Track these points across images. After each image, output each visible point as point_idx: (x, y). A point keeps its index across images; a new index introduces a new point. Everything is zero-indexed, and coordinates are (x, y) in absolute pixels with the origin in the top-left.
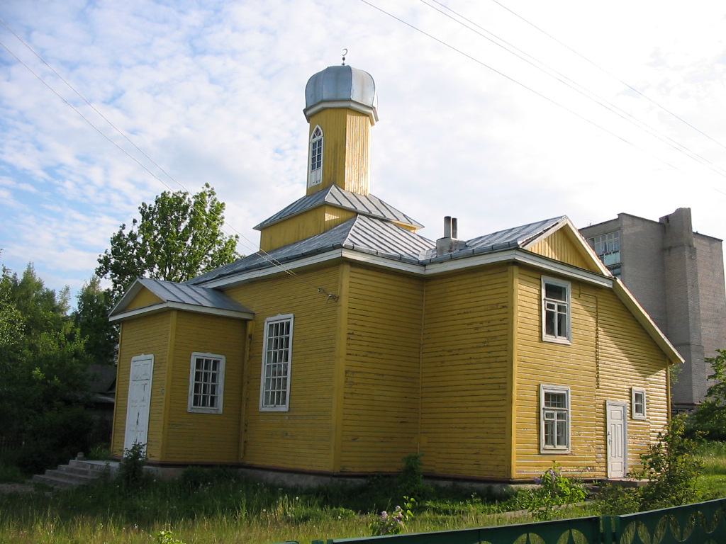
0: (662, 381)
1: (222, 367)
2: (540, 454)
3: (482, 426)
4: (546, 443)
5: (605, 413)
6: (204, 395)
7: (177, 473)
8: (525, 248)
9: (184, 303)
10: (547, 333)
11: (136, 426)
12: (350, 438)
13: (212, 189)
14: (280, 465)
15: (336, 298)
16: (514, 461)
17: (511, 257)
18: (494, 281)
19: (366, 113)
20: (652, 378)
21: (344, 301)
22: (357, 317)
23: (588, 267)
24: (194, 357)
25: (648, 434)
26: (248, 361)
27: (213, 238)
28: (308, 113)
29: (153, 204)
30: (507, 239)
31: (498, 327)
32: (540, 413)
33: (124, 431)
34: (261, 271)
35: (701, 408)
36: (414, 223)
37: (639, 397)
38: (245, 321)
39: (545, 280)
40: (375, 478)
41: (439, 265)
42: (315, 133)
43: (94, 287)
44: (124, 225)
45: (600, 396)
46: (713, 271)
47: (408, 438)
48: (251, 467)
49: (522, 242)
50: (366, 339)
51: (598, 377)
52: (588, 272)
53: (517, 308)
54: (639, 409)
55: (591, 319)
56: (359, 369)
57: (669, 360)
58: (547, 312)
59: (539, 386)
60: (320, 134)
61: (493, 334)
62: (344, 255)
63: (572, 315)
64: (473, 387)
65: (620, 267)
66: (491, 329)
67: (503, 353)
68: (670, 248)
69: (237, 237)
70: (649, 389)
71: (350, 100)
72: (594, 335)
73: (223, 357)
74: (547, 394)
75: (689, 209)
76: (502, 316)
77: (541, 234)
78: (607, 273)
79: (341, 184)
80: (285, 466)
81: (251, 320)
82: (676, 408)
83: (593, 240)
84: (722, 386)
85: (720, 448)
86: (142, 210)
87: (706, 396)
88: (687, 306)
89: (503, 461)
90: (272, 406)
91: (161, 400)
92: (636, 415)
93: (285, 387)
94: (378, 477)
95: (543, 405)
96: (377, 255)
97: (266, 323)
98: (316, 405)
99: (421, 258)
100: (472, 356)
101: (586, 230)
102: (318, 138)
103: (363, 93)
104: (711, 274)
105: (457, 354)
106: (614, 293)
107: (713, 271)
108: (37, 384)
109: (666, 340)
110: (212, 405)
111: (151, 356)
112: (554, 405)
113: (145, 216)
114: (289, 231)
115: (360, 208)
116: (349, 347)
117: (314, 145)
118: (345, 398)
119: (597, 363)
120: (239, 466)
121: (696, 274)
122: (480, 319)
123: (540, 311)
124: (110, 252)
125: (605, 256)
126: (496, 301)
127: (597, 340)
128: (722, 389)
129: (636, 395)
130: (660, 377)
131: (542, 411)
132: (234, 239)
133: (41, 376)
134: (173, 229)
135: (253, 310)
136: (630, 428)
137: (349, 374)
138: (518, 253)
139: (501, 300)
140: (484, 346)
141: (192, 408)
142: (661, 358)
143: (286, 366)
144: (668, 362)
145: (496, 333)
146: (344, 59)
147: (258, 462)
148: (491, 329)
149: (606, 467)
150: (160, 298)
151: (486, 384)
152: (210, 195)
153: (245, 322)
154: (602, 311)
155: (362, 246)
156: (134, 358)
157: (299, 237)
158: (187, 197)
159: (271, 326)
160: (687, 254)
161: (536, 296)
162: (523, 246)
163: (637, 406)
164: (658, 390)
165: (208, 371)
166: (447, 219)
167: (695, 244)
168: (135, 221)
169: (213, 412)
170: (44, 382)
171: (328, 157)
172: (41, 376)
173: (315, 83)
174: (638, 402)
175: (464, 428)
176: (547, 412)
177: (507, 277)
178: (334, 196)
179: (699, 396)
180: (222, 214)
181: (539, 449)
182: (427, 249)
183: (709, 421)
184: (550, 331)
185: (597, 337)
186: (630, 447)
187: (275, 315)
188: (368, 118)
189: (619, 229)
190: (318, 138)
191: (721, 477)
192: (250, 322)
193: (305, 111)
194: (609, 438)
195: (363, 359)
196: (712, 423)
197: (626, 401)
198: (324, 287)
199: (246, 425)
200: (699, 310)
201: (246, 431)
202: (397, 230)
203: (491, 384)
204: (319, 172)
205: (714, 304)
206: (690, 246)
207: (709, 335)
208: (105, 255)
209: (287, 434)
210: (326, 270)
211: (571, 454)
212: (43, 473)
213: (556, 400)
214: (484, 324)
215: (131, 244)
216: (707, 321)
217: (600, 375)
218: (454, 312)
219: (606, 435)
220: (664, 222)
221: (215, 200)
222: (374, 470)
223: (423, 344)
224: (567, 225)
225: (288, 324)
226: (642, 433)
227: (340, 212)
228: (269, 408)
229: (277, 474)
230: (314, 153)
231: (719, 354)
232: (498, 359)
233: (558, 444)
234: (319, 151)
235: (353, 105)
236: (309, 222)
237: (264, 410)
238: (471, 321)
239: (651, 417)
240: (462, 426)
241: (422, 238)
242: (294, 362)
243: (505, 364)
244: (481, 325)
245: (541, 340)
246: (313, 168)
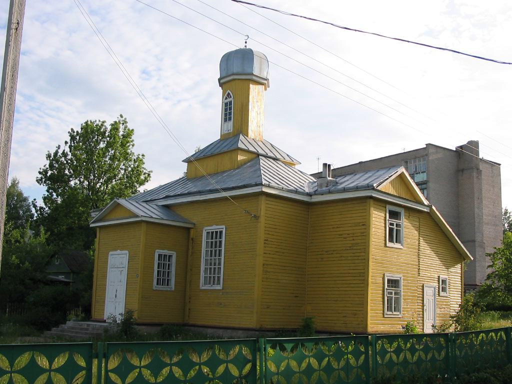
0: (458, 271)
1: (174, 259)
2: (384, 317)
4: (387, 311)
6: (163, 279)
7: (154, 330)
8: (379, 188)
10: (390, 241)
11: (114, 300)
13: (125, 119)
15: (256, 217)
16: (369, 322)
17: (369, 194)
18: (358, 208)
19: (262, 82)
20: (452, 270)
21: (262, 219)
23: (415, 199)
24: (158, 252)
26: (191, 255)
27: (126, 156)
28: (221, 81)
29: (80, 131)
31: (360, 238)
32: (384, 292)
34: (202, 196)
35: (482, 288)
36: (295, 161)
37: (444, 282)
39: (389, 207)
40: (281, 332)
42: (226, 96)
43: (14, 187)
44: (59, 146)
45: (420, 281)
46: (493, 187)
48: (194, 326)
49: (376, 184)
50: (275, 243)
51: (419, 269)
52: (416, 203)
53: (372, 226)
54: (444, 290)
55: (416, 232)
56: (271, 263)
58: (390, 228)
59: (384, 275)
60: (231, 97)
62: (263, 190)
63: (404, 230)
64: (344, 275)
67: (363, 254)
68: (463, 170)
69: (143, 155)
71: (252, 74)
72: (417, 242)
73: (175, 253)
74: (388, 280)
76: (363, 231)
77: (388, 179)
78: (426, 202)
79: (246, 134)
81: (192, 228)
82: (468, 286)
85: (493, 316)
86: (71, 134)
87: (486, 280)
88: (474, 214)
89: (362, 321)
90: (210, 285)
94: (282, 331)
95: (386, 287)
96: (282, 189)
97: (204, 231)
99: (307, 190)
102: (229, 100)
103: (261, 69)
105: (332, 254)
106: (430, 215)
107: (493, 187)
108: (13, 267)
109: (462, 245)
110: (168, 285)
112: (392, 287)
113: (73, 138)
114: (211, 165)
115: (261, 152)
117: (226, 104)
118: (263, 281)
119: (419, 260)
120: (185, 325)
121: (481, 190)
123: (385, 227)
124: (47, 166)
125: (415, 175)
126: (359, 221)
128: (496, 275)
129: (442, 280)
130: (457, 269)
131: (385, 290)
132: (141, 157)
133: (17, 261)
134: (96, 152)
135: (194, 221)
139: (361, 221)
141: (156, 287)
143: (220, 260)
144: (462, 258)
145: (359, 241)
146: (246, 42)
149: (423, 326)
150: (135, 214)
152: (123, 124)
155: (273, 184)
156: (111, 253)
157: (217, 170)
158: (105, 124)
159: (208, 233)
160: (475, 174)
161: (383, 218)
163: (442, 287)
164: (456, 277)
167: (481, 168)
168: (66, 143)
169: (169, 289)
171: (235, 112)
172: (17, 261)
173: (227, 59)
174: (443, 285)
175: (336, 301)
178: (243, 143)
179: (480, 278)
182: (307, 182)
183: (479, 297)
184: (391, 240)
185: (419, 243)
187: (212, 226)
188: (263, 86)
190: (229, 100)
192: (192, 230)
193: (219, 80)
194: (425, 308)
196: (489, 299)
197: (436, 284)
198: (247, 209)
199: (190, 298)
200: (482, 216)
201: (190, 302)
202: (283, 165)
204: (230, 125)
206: (477, 169)
207: (491, 238)
209: (221, 304)
213: (394, 283)
214: (351, 235)
216: (488, 224)
217: (421, 268)
219: (423, 306)
225: (221, 232)
226: (446, 305)
228: (207, 287)
229: (215, 330)
230: (226, 110)
231: (495, 250)
233: (395, 311)
234: (230, 109)
235: (254, 78)
236: (225, 162)
237: (203, 288)
238: (341, 233)
241: (301, 172)
242: (226, 257)
243: (364, 261)
244: (348, 236)
246: (226, 120)
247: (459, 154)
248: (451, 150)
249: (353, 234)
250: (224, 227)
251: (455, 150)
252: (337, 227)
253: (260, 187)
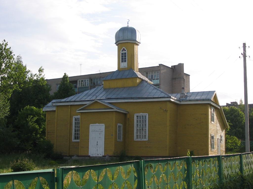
25: (222, 146)
33: (88, 148)
34: (134, 100)
68: (175, 79)
71: (136, 41)
75: (183, 64)
83: (131, 68)
102: (124, 52)
105: (190, 126)
135: (128, 111)
146: (128, 23)
153: (125, 114)
156: (91, 125)
160: (182, 82)
175: (193, 145)
180: (15, 57)
190: (124, 52)
191: (144, 188)
209: (147, 147)
220: (174, 68)
234: (125, 56)
235: (137, 42)
247: (173, 70)
248: (169, 67)
249: (201, 118)
250: (147, 114)
251: (171, 67)
252: (193, 115)
253: (170, 98)
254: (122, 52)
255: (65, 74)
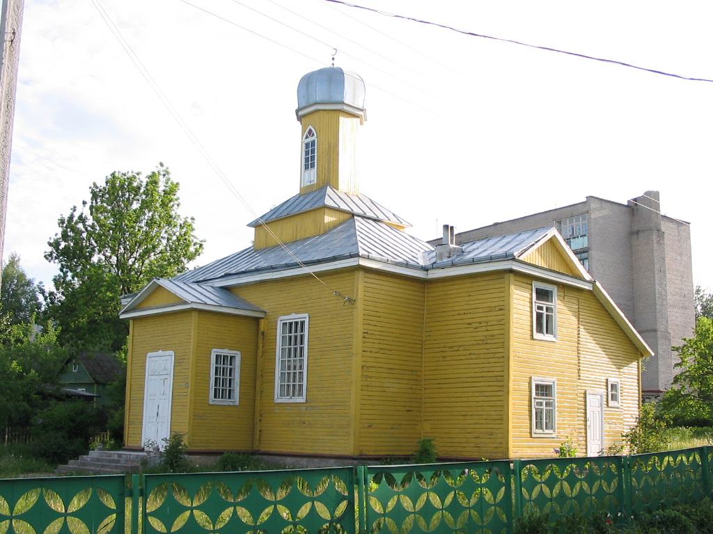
2: (531, 437)
3: (482, 413)
4: (536, 428)
5: (585, 402)
6: (223, 389)
8: (520, 258)
9: (206, 304)
10: (537, 332)
11: (155, 419)
12: (366, 425)
13: (167, 168)
14: (295, 450)
15: (352, 301)
20: (625, 369)
21: (360, 304)
22: (372, 318)
23: (572, 272)
25: (621, 419)
27: (169, 220)
28: (300, 113)
30: (501, 247)
31: (496, 327)
32: (531, 402)
33: (141, 423)
34: (274, 273)
35: (667, 396)
38: (257, 320)
39: (536, 285)
41: (441, 271)
44: (75, 207)
47: (414, 425)
50: (378, 337)
51: (579, 370)
52: (572, 277)
54: (614, 398)
55: (574, 318)
57: (641, 353)
58: (537, 313)
59: (530, 378)
60: (313, 135)
61: (490, 333)
65: (587, 252)
66: (489, 328)
67: (501, 350)
68: (638, 232)
69: (193, 219)
70: (623, 380)
71: (343, 103)
73: (239, 353)
74: (537, 386)
78: (587, 277)
80: (299, 451)
82: (647, 394)
84: (687, 374)
85: (684, 434)
87: (672, 384)
90: (289, 397)
91: (185, 394)
92: (611, 403)
93: (301, 379)
95: (534, 395)
97: (279, 322)
98: (327, 394)
99: (422, 263)
100: (472, 352)
101: (553, 212)
102: (310, 139)
104: (679, 258)
111: (172, 353)
112: (542, 395)
114: (288, 230)
115: (356, 210)
116: (364, 345)
117: (307, 145)
120: (254, 453)
122: (480, 320)
123: (532, 312)
125: (572, 240)
127: (579, 337)
129: (612, 385)
130: (632, 369)
131: (533, 400)
132: (189, 221)
133: (19, 369)
135: (265, 309)
136: (606, 414)
137: (365, 369)
138: (514, 263)
140: (483, 344)
141: (213, 401)
142: (635, 351)
144: (639, 356)
145: (495, 333)
146: (333, 59)
147: (264, 449)
148: (489, 328)
149: (586, 449)
151: (485, 377)
152: (164, 175)
153: (257, 320)
154: (583, 311)
155: (374, 255)
156: (149, 354)
161: (528, 300)
162: (519, 256)
165: (225, 366)
166: (446, 227)
167: (663, 229)
169: (231, 404)
170: (20, 376)
171: (320, 155)
172: (19, 369)
173: (308, 82)
176: (537, 400)
177: (504, 283)
179: (665, 382)
181: (531, 433)
184: (540, 330)
185: (579, 334)
186: (606, 431)
187: (289, 314)
188: (358, 119)
189: (587, 212)
190: (310, 139)
193: (297, 112)
195: (378, 355)
196: (677, 411)
201: (260, 420)
203: (490, 377)
205: (681, 289)
208: (56, 238)
209: (304, 423)
210: (342, 275)
211: (557, 438)
212: (66, 463)
213: (544, 390)
214: (483, 324)
215: (80, 226)
216: (674, 306)
217: (581, 368)
218: (456, 313)
221: (168, 180)
222: (386, 453)
223: (425, 341)
224: (554, 236)
225: (303, 323)
226: (617, 419)
227: (338, 214)
228: (285, 400)
229: (298, 459)
230: (307, 153)
231: (685, 343)
232: (496, 355)
234: (313, 151)
235: (346, 108)
236: (306, 226)
239: (624, 405)
240: (464, 413)
243: (501, 360)
245: (532, 338)
246: (307, 167)
250: (307, 315)
254: (313, 138)
255: (249, 225)
